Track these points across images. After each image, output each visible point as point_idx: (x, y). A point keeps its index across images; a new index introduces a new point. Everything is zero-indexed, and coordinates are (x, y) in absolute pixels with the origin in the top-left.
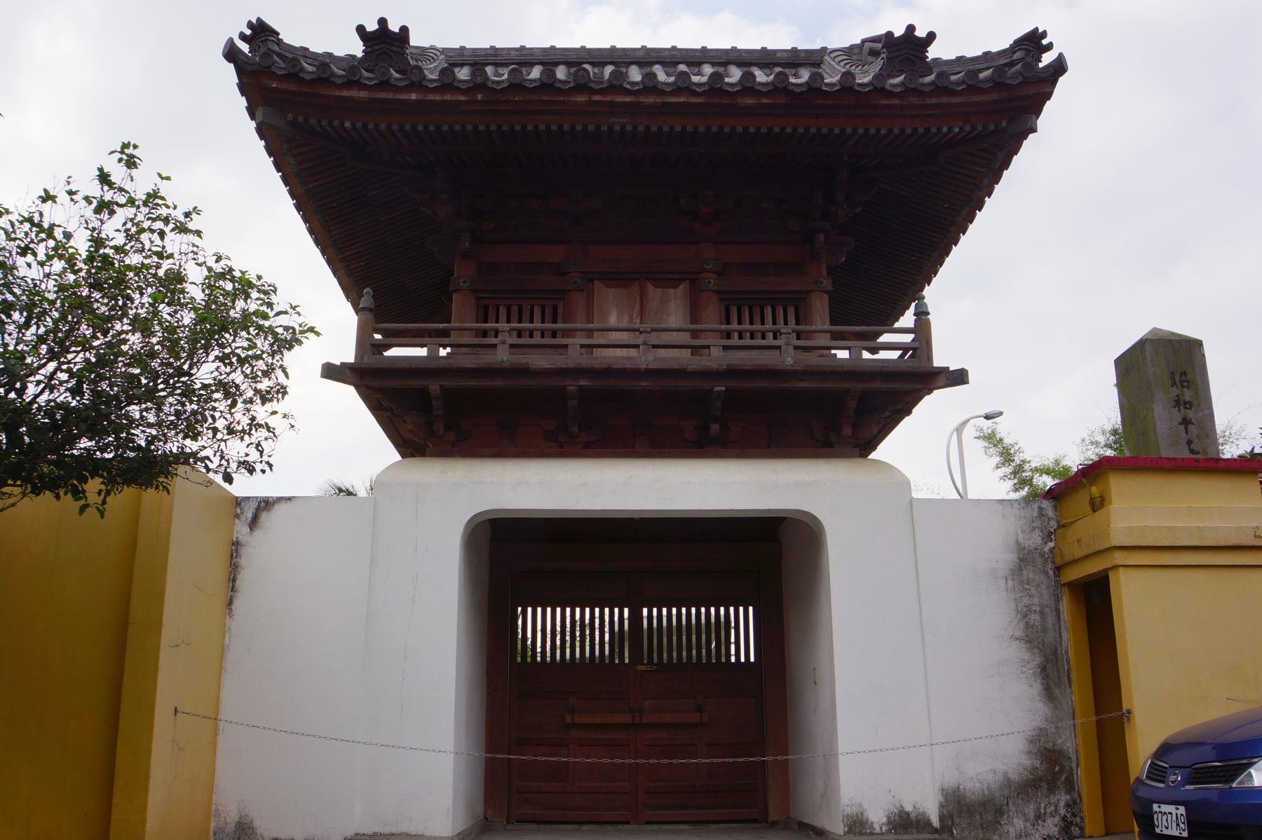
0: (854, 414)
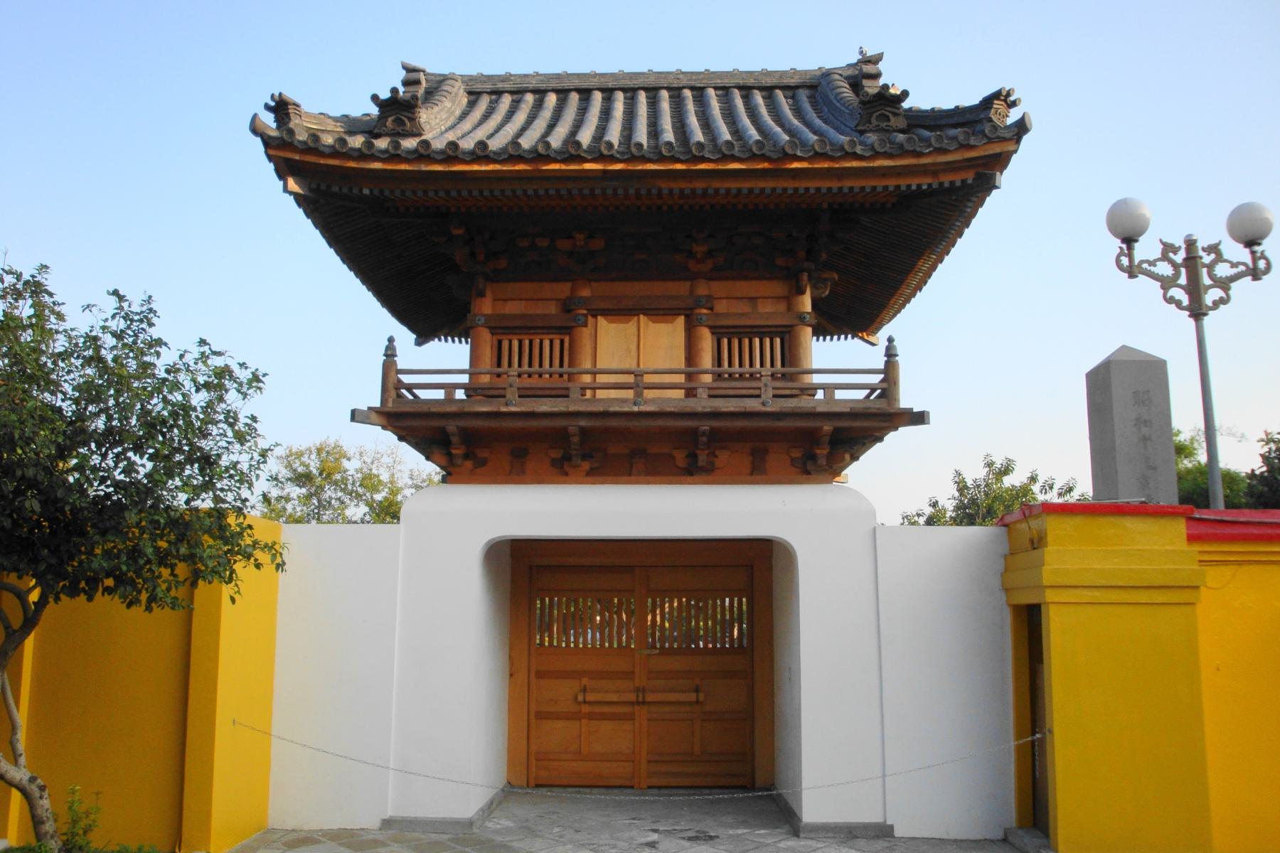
0: (825, 442)
